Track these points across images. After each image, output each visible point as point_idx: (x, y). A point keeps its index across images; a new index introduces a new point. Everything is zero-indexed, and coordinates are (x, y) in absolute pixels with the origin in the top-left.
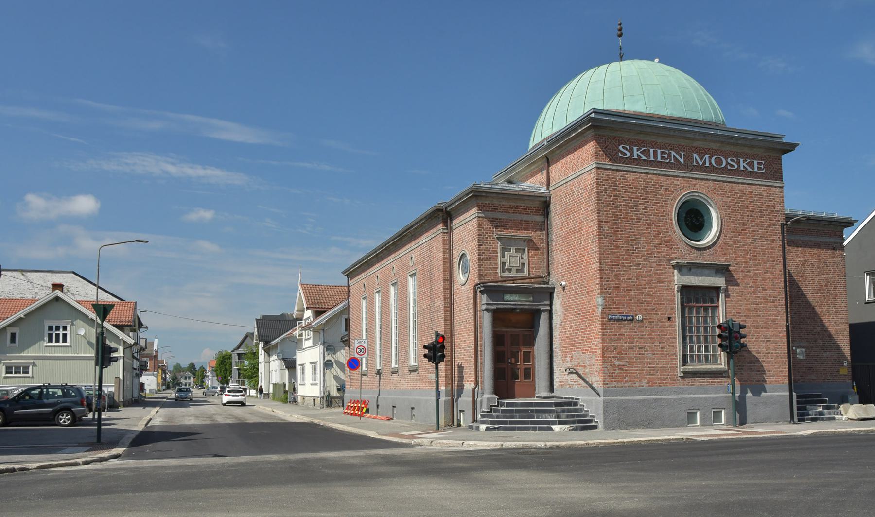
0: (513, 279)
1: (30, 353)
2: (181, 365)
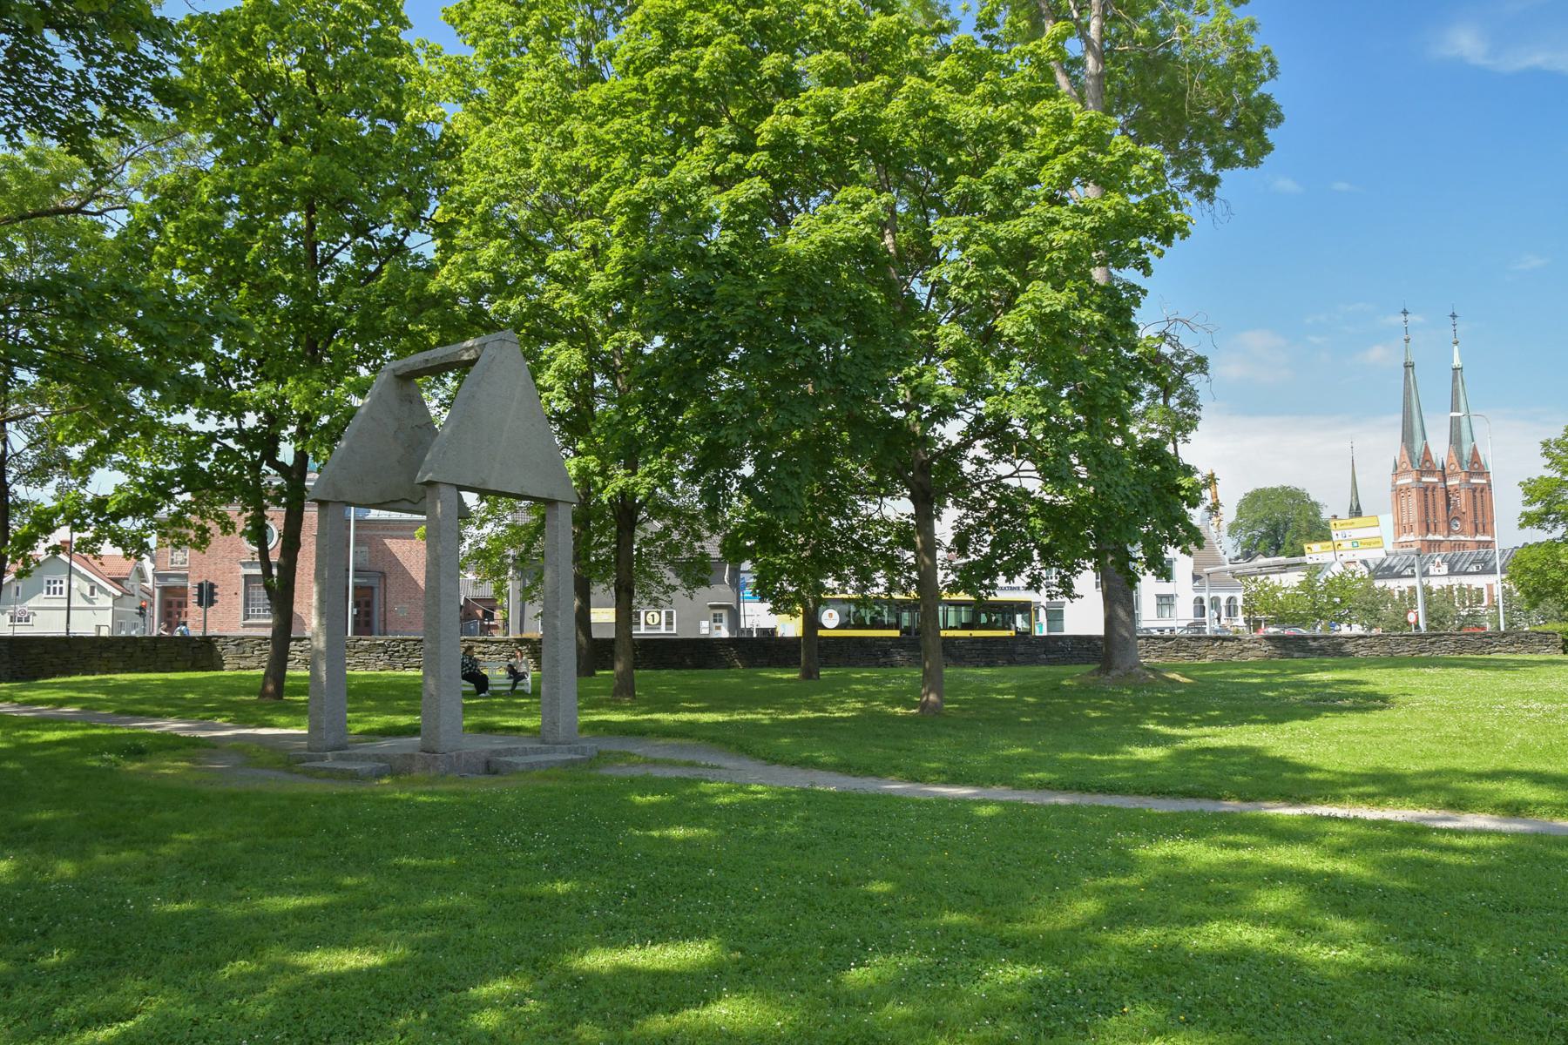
0: (178, 569)
1: (32, 603)
2: (704, 588)
